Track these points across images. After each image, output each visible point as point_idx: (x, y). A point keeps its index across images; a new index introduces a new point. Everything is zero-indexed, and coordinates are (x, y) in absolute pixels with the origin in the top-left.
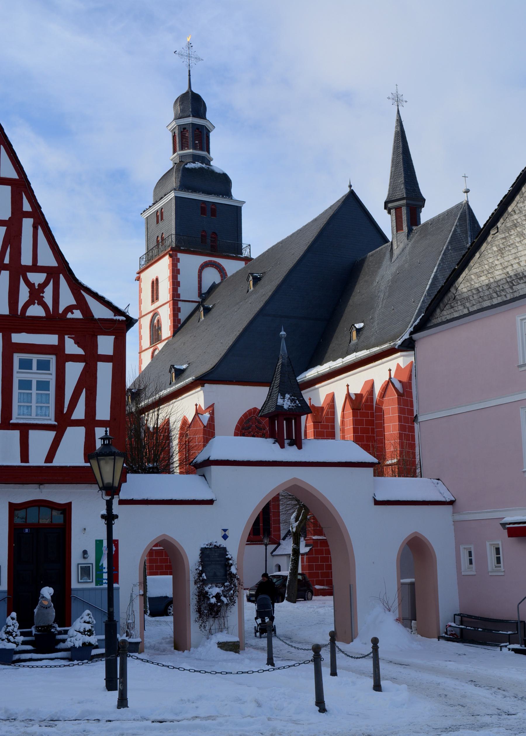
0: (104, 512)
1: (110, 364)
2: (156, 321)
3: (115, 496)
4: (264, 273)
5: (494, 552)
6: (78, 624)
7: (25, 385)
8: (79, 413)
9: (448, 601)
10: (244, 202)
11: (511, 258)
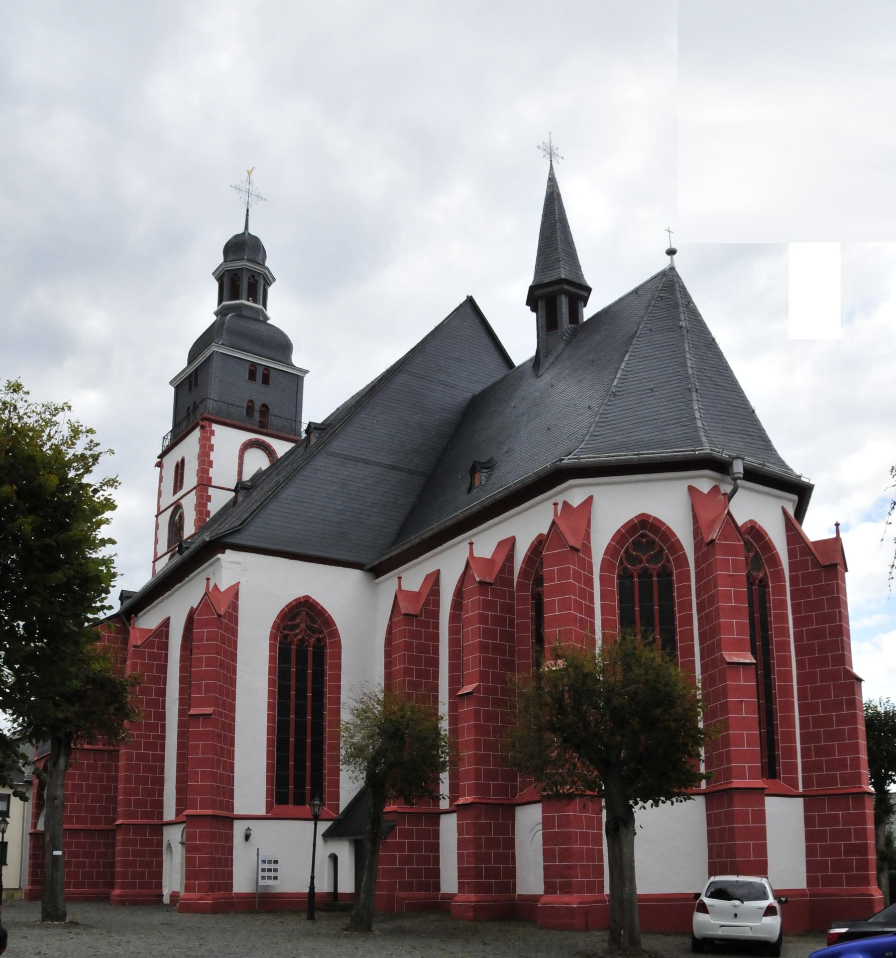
2: (177, 518)
3: (345, 851)
10: (306, 372)
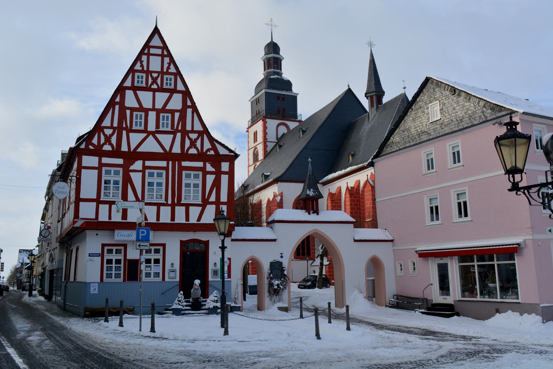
0: (221, 245)
1: (227, 176)
4: (307, 128)
5: (412, 264)
6: (211, 297)
7: (188, 185)
8: (213, 198)
9: (390, 289)
11: (419, 123)
